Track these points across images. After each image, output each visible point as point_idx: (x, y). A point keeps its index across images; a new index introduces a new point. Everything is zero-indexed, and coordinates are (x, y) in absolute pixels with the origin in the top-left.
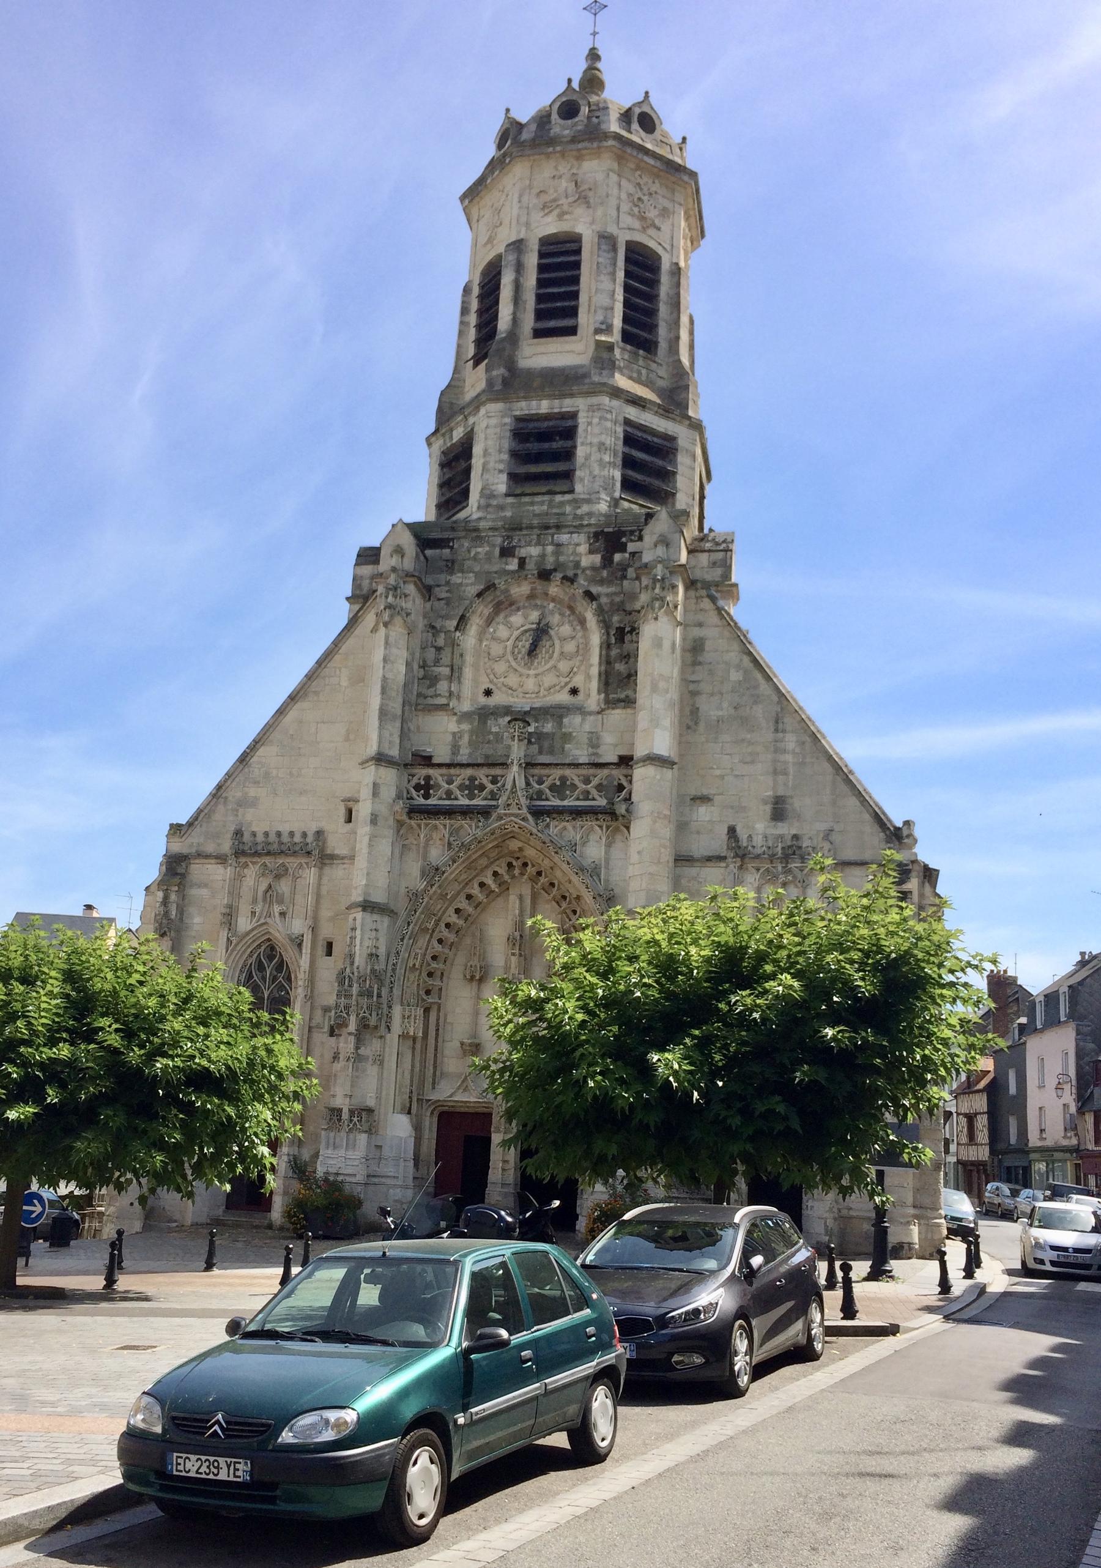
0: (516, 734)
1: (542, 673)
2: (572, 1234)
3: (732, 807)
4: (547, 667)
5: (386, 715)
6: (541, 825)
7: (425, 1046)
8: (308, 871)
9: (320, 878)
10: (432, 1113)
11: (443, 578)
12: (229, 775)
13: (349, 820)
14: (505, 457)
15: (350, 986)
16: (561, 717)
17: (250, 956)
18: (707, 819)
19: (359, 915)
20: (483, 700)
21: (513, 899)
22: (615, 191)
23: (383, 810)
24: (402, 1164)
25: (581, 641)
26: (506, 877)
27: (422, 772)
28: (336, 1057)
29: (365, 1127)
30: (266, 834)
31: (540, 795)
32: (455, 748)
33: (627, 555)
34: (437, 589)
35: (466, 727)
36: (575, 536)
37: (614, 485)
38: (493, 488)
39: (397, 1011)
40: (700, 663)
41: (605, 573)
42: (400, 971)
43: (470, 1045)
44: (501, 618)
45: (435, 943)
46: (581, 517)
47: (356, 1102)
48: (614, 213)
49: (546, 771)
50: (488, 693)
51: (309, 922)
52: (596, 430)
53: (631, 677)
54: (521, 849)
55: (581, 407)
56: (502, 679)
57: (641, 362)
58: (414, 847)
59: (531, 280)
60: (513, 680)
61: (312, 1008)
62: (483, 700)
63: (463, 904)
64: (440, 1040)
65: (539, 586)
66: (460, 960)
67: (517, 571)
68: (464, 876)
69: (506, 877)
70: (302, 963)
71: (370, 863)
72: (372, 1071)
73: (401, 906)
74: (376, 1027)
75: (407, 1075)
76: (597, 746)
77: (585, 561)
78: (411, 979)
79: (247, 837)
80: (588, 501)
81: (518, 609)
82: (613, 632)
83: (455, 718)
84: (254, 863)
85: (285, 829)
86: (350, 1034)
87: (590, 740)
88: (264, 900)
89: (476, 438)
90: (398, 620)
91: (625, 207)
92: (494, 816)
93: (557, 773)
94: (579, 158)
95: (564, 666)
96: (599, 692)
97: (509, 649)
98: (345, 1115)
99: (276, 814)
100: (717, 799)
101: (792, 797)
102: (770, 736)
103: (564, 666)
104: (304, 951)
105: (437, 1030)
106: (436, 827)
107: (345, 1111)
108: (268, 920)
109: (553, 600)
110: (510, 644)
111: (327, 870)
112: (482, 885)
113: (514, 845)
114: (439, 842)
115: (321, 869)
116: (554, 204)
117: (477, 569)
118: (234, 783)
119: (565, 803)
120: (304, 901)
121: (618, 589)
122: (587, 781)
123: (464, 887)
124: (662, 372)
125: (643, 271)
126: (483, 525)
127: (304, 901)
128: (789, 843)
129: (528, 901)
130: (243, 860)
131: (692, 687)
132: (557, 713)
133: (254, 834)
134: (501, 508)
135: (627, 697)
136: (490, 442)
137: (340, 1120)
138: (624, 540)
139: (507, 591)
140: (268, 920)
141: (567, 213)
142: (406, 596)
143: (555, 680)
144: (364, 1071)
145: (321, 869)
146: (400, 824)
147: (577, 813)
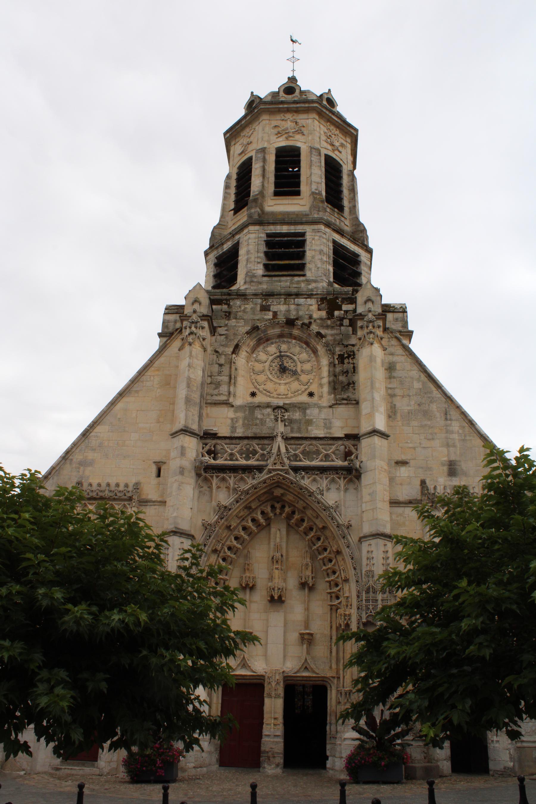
2: (324, 771)
3: (422, 468)
5: (190, 402)
12: (75, 445)
13: (159, 475)
14: (262, 255)
18: (406, 475)
20: (250, 399)
22: (318, 129)
27: (211, 442)
32: (233, 428)
33: (343, 312)
34: (219, 329)
35: (240, 415)
36: (309, 300)
37: (329, 274)
38: (254, 272)
40: (394, 378)
41: (329, 322)
48: (318, 139)
50: (253, 394)
52: (318, 243)
53: (351, 385)
54: (282, 495)
55: (308, 230)
57: (336, 215)
59: (271, 167)
60: (270, 386)
62: (250, 399)
65: (286, 330)
67: (272, 319)
68: (242, 514)
76: (330, 428)
77: (316, 315)
80: (315, 281)
81: (272, 343)
82: (336, 357)
83: (233, 409)
85: (113, 482)
87: (325, 424)
89: (241, 246)
91: (324, 138)
96: (330, 393)
97: (267, 368)
100: (412, 463)
101: (460, 461)
102: (442, 422)
109: (295, 338)
110: (268, 364)
113: (278, 492)
118: (78, 450)
121: (338, 332)
124: (347, 222)
125: (333, 172)
131: (390, 391)
132: (302, 407)
133: (91, 485)
141: (291, 137)
143: (299, 387)
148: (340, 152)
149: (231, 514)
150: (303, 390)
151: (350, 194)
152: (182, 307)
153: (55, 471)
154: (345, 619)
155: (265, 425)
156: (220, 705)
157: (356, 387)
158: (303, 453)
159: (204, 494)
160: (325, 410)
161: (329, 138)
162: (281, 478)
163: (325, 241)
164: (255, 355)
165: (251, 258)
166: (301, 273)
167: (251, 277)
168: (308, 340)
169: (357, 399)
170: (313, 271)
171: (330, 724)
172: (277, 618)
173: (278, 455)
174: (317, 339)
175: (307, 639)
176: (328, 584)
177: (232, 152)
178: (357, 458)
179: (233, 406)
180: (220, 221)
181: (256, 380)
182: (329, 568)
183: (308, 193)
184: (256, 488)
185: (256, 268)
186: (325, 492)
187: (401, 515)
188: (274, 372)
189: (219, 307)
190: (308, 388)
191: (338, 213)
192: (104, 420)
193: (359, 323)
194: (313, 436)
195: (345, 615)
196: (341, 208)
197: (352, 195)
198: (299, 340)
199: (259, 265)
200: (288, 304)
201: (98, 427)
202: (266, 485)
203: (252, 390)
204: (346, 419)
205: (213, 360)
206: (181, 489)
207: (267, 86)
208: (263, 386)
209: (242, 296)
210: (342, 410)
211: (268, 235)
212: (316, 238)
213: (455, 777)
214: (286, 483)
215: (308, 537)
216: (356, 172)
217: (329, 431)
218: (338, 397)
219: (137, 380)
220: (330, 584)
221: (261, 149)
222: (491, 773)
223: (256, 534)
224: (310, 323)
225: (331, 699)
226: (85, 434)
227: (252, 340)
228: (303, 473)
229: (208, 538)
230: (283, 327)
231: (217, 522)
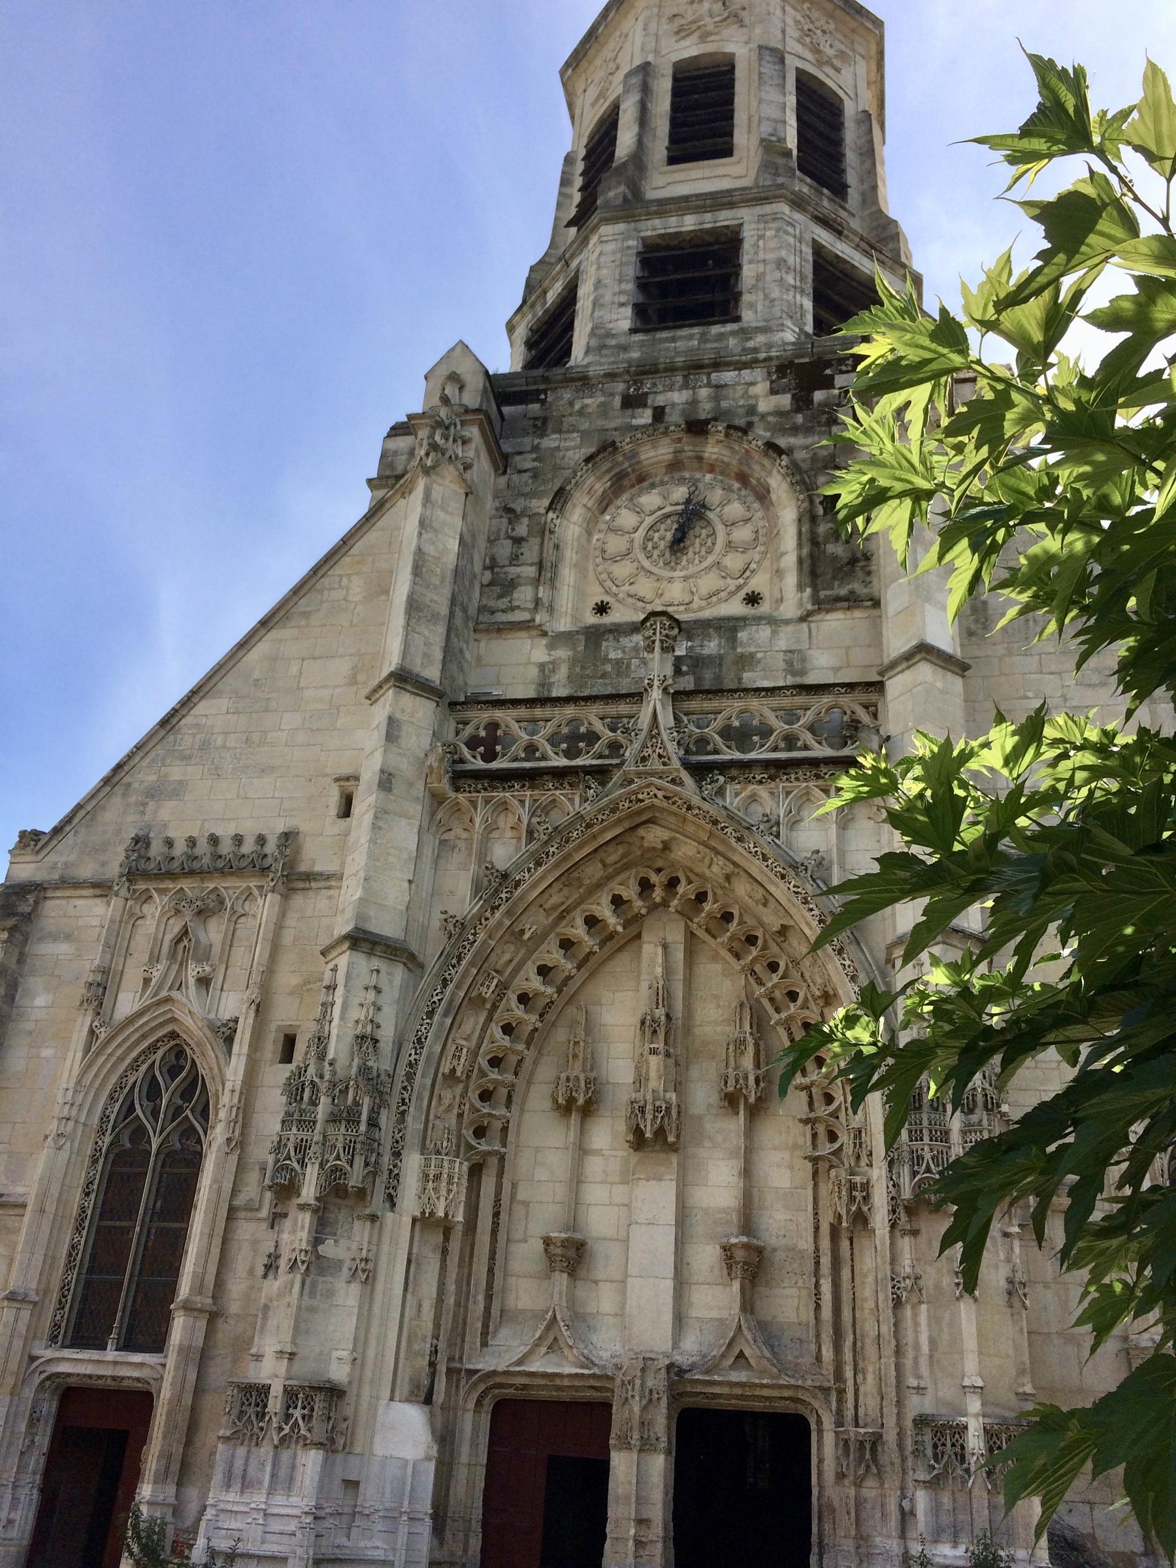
0: (658, 637)
4: (704, 565)
5: (418, 609)
6: (708, 789)
7: (466, 1242)
8: (260, 901)
9: (283, 914)
10: (479, 1403)
11: (527, 442)
14: (630, 286)
15: (314, 1103)
16: (734, 630)
17: (134, 1066)
19: (344, 959)
21: (650, 950)
22: (779, 12)
23: (404, 765)
24: (403, 1530)
28: (271, 1267)
29: (319, 1429)
30: (192, 842)
34: (518, 458)
35: (562, 653)
39: (413, 1162)
41: (799, 419)
42: (422, 1080)
43: (566, 1243)
45: (496, 1031)
46: (756, 350)
47: (305, 1370)
49: (715, 704)
50: (602, 609)
51: (254, 993)
52: (773, 244)
54: (666, 846)
58: (462, 845)
59: (662, 104)
60: (645, 587)
61: (241, 1168)
62: (592, 619)
63: (553, 955)
64: (498, 1274)
66: (546, 1072)
68: (555, 899)
69: (638, 905)
70: (229, 1073)
72: (348, 1295)
73: (431, 951)
74: (361, 1194)
77: (763, 406)
78: (446, 1101)
79: (156, 849)
81: (653, 486)
83: (544, 641)
84: (161, 892)
85: (225, 831)
86: (302, 1207)
87: (789, 663)
88: (172, 955)
92: (617, 776)
94: (668, 1452)
95: (734, 562)
96: (800, 587)
98: (275, 1404)
99: (216, 806)
103: (734, 562)
104: (236, 1048)
105: (496, 1215)
106: (504, 806)
107: (277, 1390)
108: (175, 994)
109: (712, 469)
110: (639, 535)
111: (298, 900)
112: (592, 922)
114: (509, 834)
115: (286, 897)
116: (694, 27)
117: (585, 425)
119: (753, 755)
120: (247, 957)
123: (556, 923)
126: (593, 371)
127: (247, 957)
129: (679, 955)
130: (141, 886)
132: (729, 627)
133: (170, 843)
134: (624, 348)
135: (852, 592)
136: (604, 272)
137: (261, 1416)
138: (828, 372)
139: (634, 455)
140: (175, 994)
142: (464, 442)
143: (721, 583)
144: (330, 1294)
145: (286, 897)
146: (437, 799)
147: (777, 769)
148: (838, 70)
149: (521, 898)
150: (733, 588)
151: (862, 163)
153: (82, 813)
154: (852, 1199)
155: (627, 676)
156: (481, 1472)
157: (873, 568)
159: (454, 848)
160: (790, 628)
162: (660, 794)
163: (792, 240)
165: (602, 296)
167: (602, 338)
168: (745, 468)
169: (876, 594)
170: (760, 307)
171: (820, 1543)
172: (657, 1197)
173: (652, 737)
174: (766, 462)
175: (750, 1265)
177: (577, 112)
179: (544, 634)
181: (609, 574)
183: (755, 141)
184: (588, 826)
185: (615, 317)
186: (783, 830)
188: (656, 553)
189: (520, 408)
190: (745, 584)
191: (831, 200)
192: (219, 686)
195: (852, 1187)
196: (839, 190)
197: (868, 164)
198: (722, 473)
199: (622, 310)
200: (694, 388)
201: (203, 703)
202: (617, 816)
204: (848, 648)
205: (499, 530)
206: (380, 828)
208: (627, 587)
209: (583, 382)
210: (835, 622)
212: (769, 233)
214: (674, 808)
215: (742, 962)
218: (822, 594)
219: (307, 587)
224: (750, 425)
225: (821, 1461)
226: (168, 722)
227: (599, 478)
228: (722, 779)
229: (454, 961)
230: (679, 440)
231: (480, 918)
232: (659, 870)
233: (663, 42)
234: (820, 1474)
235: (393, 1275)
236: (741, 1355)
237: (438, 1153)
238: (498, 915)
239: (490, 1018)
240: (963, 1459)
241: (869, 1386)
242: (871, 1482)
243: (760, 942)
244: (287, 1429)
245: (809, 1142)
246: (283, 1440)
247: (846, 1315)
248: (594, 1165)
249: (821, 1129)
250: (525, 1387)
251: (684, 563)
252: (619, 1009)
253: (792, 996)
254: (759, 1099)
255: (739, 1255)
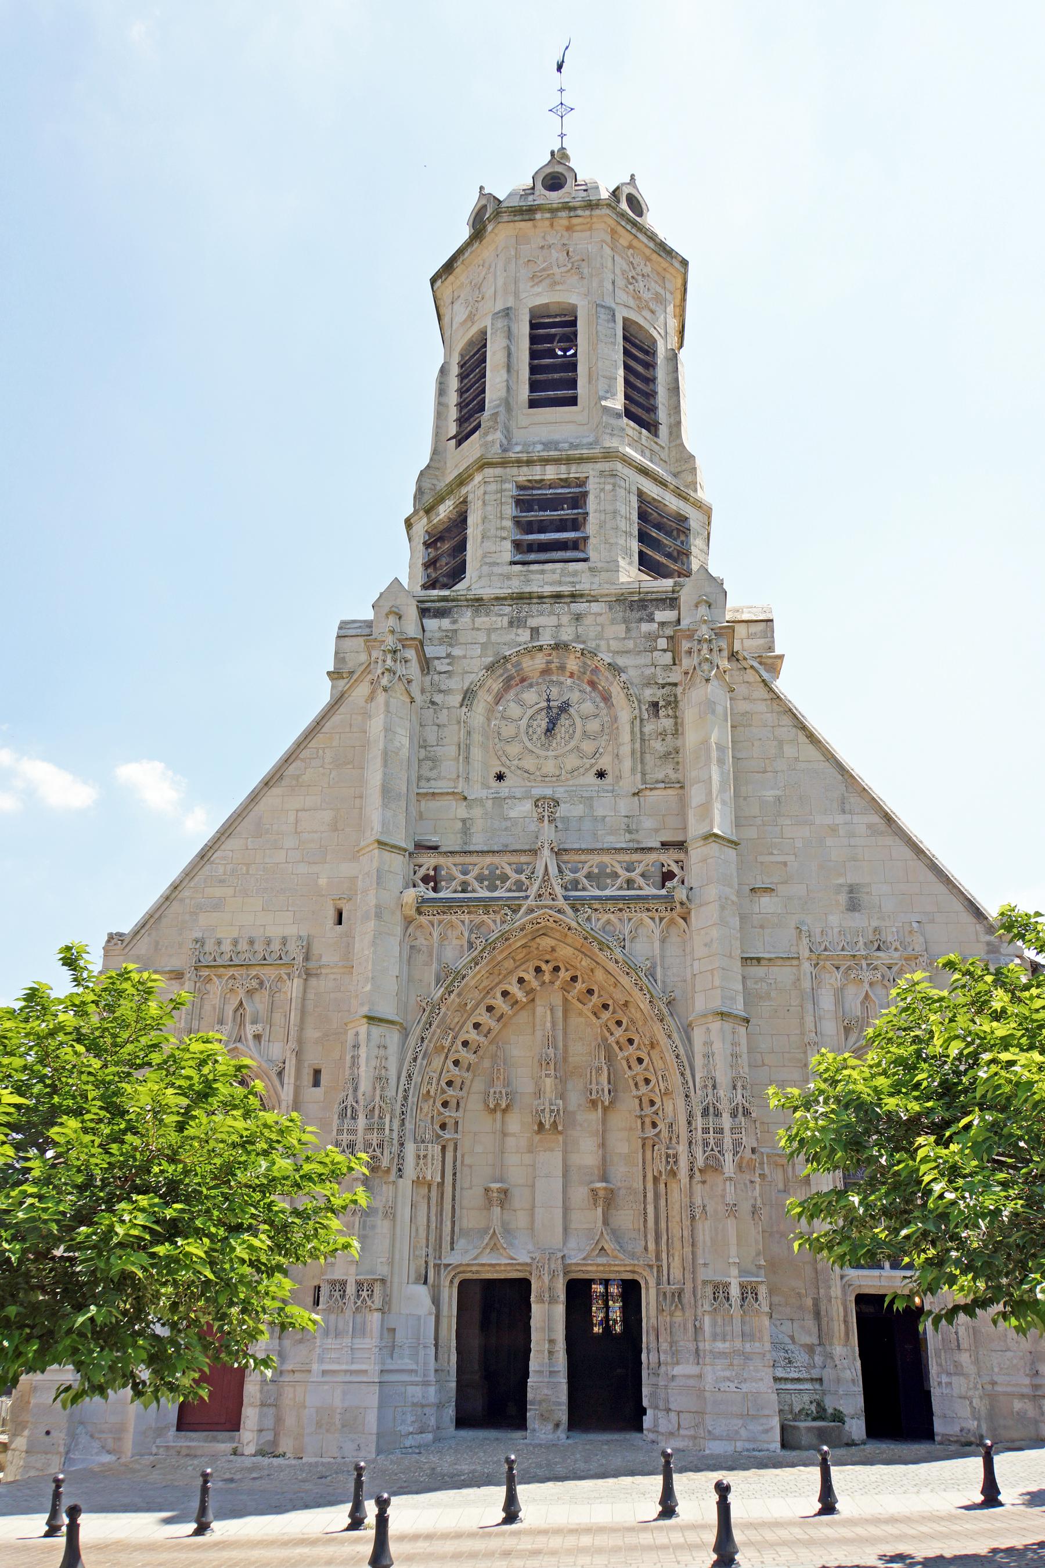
0: (546, 814)
1: (563, 755)
4: (568, 748)
10: (451, 1282)
14: (509, 523)
21: (540, 1009)
22: (610, 264)
25: (606, 719)
26: (535, 984)
27: (429, 862)
31: (575, 885)
33: (656, 625)
34: (436, 662)
44: (511, 695)
48: (610, 287)
51: (293, 1044)
54: (553, 949)
55: (591, 473)
56: (516, 762)
60: (529, 763)
63: (484, 1018)
68: (485, 983)
69: (535, 984)
71: (373, 970)
75: (422, 1234)
78: (425, 1110)
79: (209, 947)
81: (531, 686)
90: (400, 688)
91: (621, 282)
93: (596, 859)
98: (351, 1289)
99: (245, 918)
100: (780, 888)
103: (588, 747)
104: (286, 1081)
110: (524, 723)
112: (505, 994)
119: (607, 892)
122: (629, 869)
125: (640, 359)
128: (871, 938)
140: (239, 1045)
143: (577, 762)
149: (466, 985)
152: (369, 624)
153: (152, 921)
154: (668, 1162)
156: (454, 1320)
158: (589, 876)
161: (631, 284)
164: (501, 708)
166: (581, 555)
168: (595, 678)
172: (551, 1161)
176: (637, 1101)
177: (446, 320)
178: (683, 883)
180: (431, 460)
182: (637, 1074)
187: (762, 980)
188: (535, 737)
190: (596, 763)
193: (685, 645)
194: (605, 846)
195: (668, 1156)
196: (651, 426)
203: (497, 770)
207: (512, 178)
211: (520, 487)
213: (874, 1447)
216: (682, 355)
217: (633, 836)
219: (294, 757)
220: (641, 1100)
221: (503, 310)
222: (937, 1438)
223: (511, 1017)
225: (648, 1304)
227: (495, 681)
230: (550, 655)
232: (547, 962)
233: (522, 286)
234: (647, 1310)
235: (404, 1212)
236: (602, 1249)
237: (423, 1142)
238: (452, 996)
239: (446, 1057)
240: (728, 1299)
241: (676, 1263)
242: (679, 1313)
243: (611, 1008)
244: (359, 1302)
245: (639, 1127)
246: (357, 1309)
247: (663, 1225)
248: (510, 1141)
249: (648, 1121)
250: (477, 1272)
251: (554, 745)
252: (522, 1049)
253: (631, 1041)
254: (610, 1103)
255: (601, 1193)
